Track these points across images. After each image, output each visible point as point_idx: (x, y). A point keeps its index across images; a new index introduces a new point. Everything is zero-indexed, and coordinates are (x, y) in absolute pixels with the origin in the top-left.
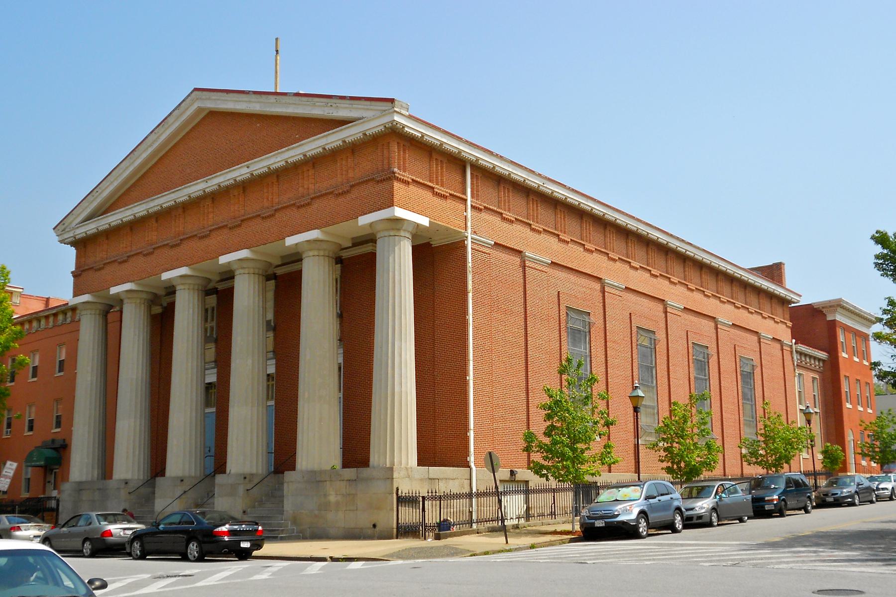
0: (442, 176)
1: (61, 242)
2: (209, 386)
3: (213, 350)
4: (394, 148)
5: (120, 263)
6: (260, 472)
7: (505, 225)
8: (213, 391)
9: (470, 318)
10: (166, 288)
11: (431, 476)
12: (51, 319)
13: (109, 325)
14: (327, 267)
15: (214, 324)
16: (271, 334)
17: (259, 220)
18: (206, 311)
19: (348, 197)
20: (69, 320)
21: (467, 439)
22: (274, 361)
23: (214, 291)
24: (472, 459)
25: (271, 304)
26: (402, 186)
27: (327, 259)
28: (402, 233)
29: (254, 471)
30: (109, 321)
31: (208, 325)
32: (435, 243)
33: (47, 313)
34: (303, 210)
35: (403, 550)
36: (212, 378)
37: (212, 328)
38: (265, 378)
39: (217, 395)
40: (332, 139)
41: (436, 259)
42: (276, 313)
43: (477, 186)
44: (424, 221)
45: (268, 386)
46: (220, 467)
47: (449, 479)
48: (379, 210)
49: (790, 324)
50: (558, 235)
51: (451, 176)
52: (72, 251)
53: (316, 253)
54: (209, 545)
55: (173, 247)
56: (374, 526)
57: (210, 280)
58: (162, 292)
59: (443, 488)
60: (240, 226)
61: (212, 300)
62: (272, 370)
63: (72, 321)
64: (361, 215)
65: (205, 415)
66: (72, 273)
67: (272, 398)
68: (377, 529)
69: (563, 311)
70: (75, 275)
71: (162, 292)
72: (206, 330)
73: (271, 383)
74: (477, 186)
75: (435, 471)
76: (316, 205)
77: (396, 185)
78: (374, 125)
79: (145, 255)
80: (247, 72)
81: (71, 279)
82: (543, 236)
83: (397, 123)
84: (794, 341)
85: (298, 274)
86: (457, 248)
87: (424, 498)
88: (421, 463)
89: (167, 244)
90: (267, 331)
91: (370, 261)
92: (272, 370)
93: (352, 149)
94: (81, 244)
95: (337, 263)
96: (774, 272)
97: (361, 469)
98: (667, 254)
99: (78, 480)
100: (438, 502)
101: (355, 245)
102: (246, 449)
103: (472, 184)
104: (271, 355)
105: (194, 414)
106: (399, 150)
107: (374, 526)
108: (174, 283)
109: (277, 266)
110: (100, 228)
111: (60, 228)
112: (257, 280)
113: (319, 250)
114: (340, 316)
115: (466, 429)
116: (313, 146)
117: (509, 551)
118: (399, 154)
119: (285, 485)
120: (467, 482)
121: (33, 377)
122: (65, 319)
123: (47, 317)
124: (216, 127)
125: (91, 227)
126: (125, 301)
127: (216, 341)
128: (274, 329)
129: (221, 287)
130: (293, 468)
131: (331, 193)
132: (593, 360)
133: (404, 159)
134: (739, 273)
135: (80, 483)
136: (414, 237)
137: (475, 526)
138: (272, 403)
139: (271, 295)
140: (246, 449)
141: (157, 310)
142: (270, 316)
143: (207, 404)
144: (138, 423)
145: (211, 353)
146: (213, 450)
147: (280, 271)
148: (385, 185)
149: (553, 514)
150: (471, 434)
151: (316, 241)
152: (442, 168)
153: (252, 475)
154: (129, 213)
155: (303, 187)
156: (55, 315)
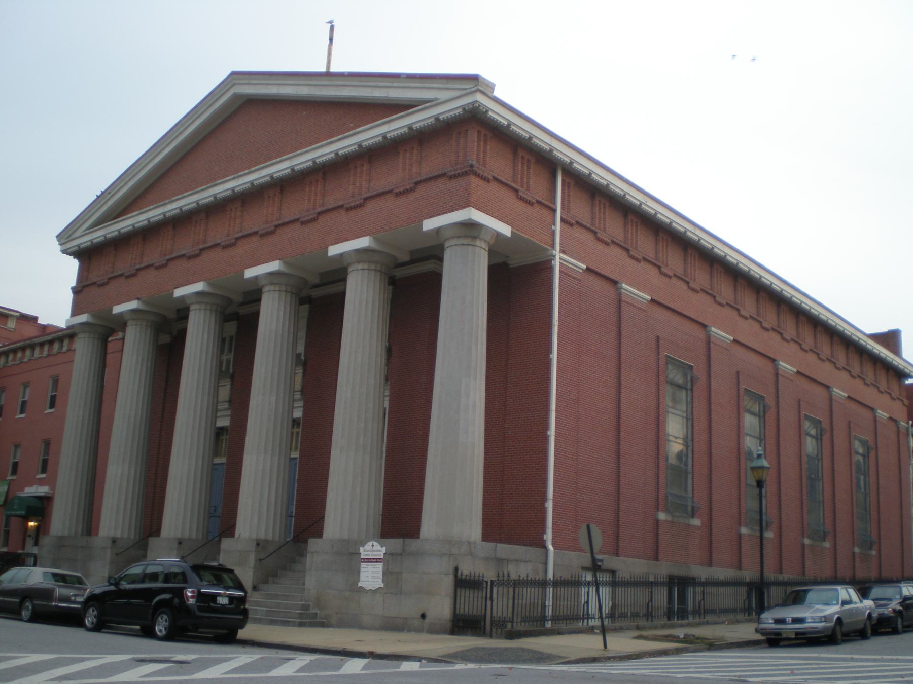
0: (528, 178)
1: (65, 252)
2: (220, 432)
3: (228, 387)
4: (473, 136)
5: (128, 277)
6: (277, 539)
7: (600, 247)
8: (224, 437)
9: (554, 356)
10: (178, 310)
11: (499, 555)
12: (46, 348)
13: (109, 357)
14: (378, 282)
15: (231, 356)
16: (300, 371)
17: (297, 226)
18: (223, 340)
19: (411, 197)
20: (65, 349)
21: (544, 511)
22: (301, 404)
23: (236, 316)
24: (549, 536)
25: (302, 334)
26: (481, 183)
27: (378, 274)
28: (478, 243)
29: (270, 537)
30: (109, 351)
31: (224, 358)
32: (514, 262)
33: (42, 340)
34: (352, 213)
35: (468, 650)
36: (224, 422)
37: (228, 362)
38: (290, 422)
39: (227, 442)
40: (396, 126)
41: (515, 282)
42: (308, 346)
43: (569, 196)
44: (505, 230)
45: (292, 433)
46: (229, 529)
47: (520, 562)
48: (450, 211)
49: (906, 402)
50: (659, 268)
51: (536, 186)
52: (73, 265)
53: (366, 266)
54: (217, 625)
55: (190, 258)
56: (423, 616)
57: (229, 301)
58: (172, 315)
59: (516, 571)
60: (273, 232)
61: (231, 328)
62: (298, 414)
63: (69, 350)
64: (426, 218)
65: (214, 467)
66: (73, 288)
67: (296, 449)
68: (427, 620)
69: (662, 362)
70: (76, 291)
71: (172, 315)
72: (221, 363)
73: (295, 430)
74: (569, 196)
75: (504, 549)
76: (370, 206)
77: (474, 180)
78: (450, 106)
79: (157, 268)
80: (290, 49)
81: (70, 296)
82: (643, 264)
83: (481, 104)
84: (911, 422)
85: (341, 297)
86: (543, 268)
87: (492, 581)
88: (486, 537)
89: (184, 255)
90: (297, 365)
91: (433, 282)
92: (298, 414)
93: (420, 138)
94: (86, 256)
95: (389, 284)
96: (891, 339)
97: (408, 541)
98: (778, 306)
99: (60, 534)
100: (511, 590)
101: (412, 262)
102: (259, 508)
103: (563, 193)
104: (298, 396)
105: (200, 463)
106: (479, 140)
107: (423, 616)
108: (188, 302)
109: (315, 286)
110: (109, 236)
111: (64, 237)
112: (289, 299)
113: (369, 262)
114: (389, 351)
115: (544, 499)
116: (371, 134)
117: (608, 659)
118: (479, 146)
119: (309, 556)
120: (541, 567)
121: (21, 413)
122: (61, 347)
123: (42, 345)
124: (247, 112)
125: (98, 235)
126: (129, 323)
127: (232, 378)
128: (305, 365)
129: (243, 311)
130: (319, 534)
131: (390, 192)
132: (696, 424)
133: (485, 152)
134: (857, 336)
135: (62, 538)
136: (492, 253)
137: (549, 625)
138: (296, 454)
139: (303, 323)
140: (259, 508)
141: (165, 339)
142: (301, 349)
143: (216, 453)
144: (133, 470)
145: (225, 392)
146: (220, 510)
147: (316, 293)
148: (462, 182)
149: (649, 615)
150: (550, 505)
151: (365, 251)
152: (529, 168)
153: (267, 541)
154: (143, 217)
155: (354, 184)
156: (51, 342)
